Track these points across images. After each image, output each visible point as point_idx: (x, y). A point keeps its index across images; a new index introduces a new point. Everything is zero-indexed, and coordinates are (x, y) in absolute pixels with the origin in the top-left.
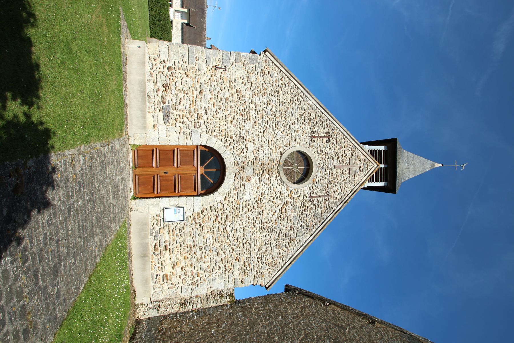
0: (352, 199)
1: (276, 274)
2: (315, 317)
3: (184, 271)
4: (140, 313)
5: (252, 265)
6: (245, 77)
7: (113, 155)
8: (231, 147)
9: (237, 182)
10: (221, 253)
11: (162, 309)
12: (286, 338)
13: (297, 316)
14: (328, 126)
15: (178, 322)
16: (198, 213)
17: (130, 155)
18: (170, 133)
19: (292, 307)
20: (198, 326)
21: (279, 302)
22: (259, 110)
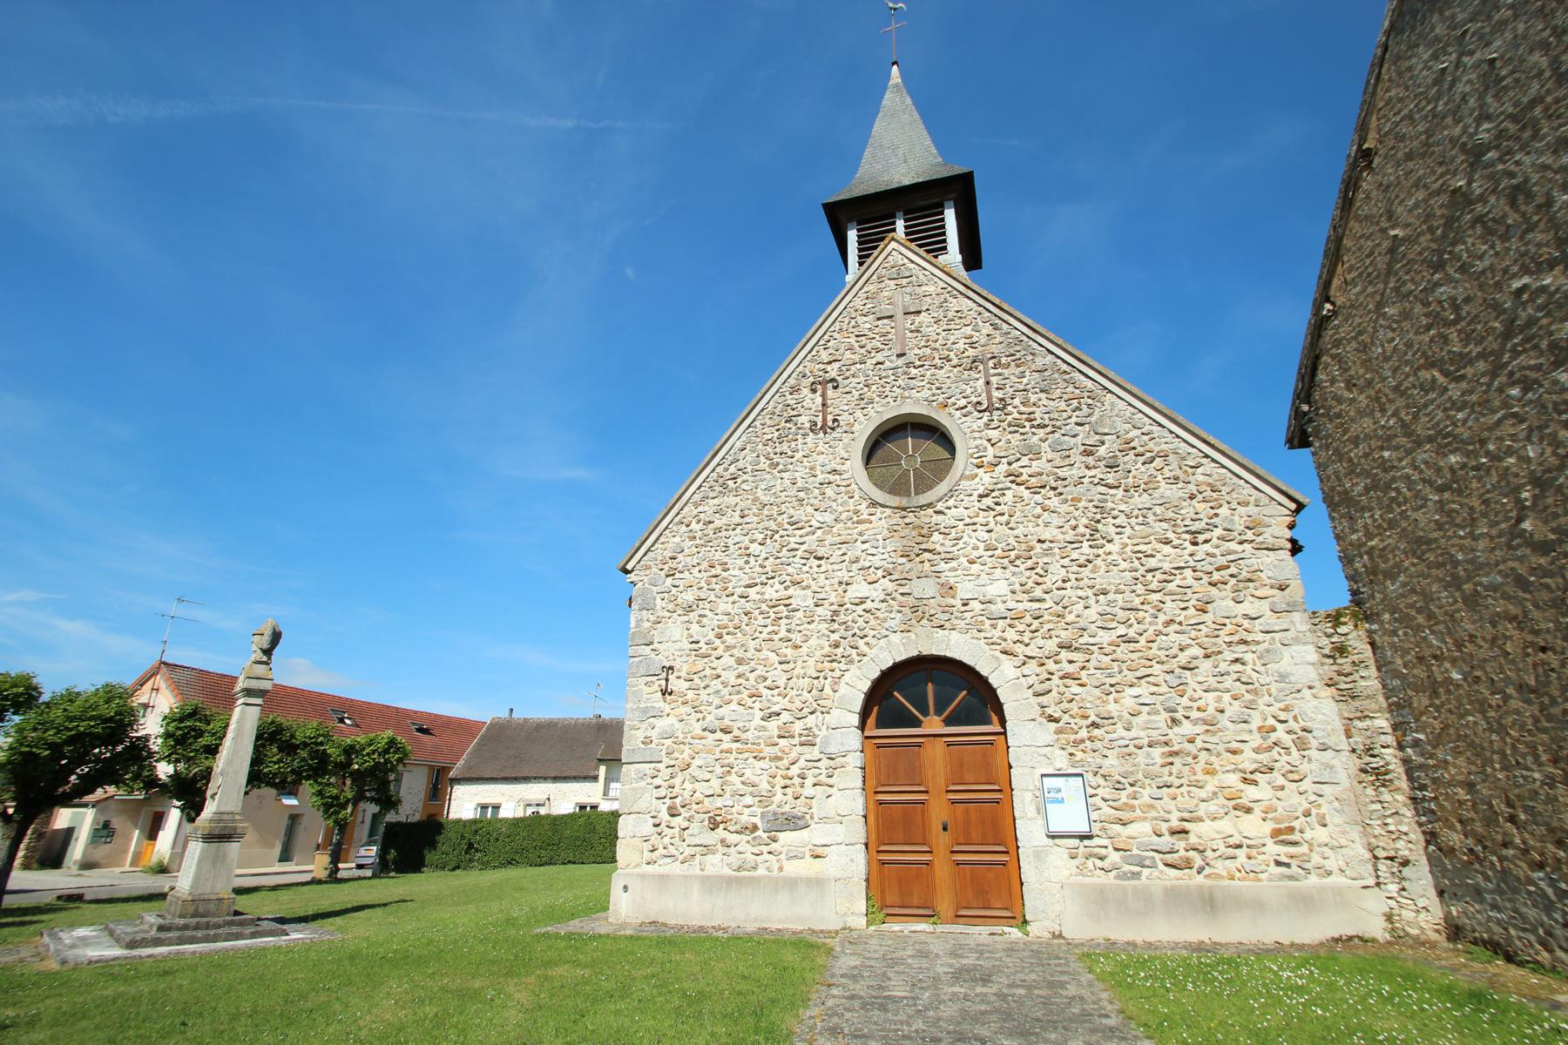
0: (990, 291)
1: (1247, 482)
2: (1373, 343)
3: (1258, 776)
4: (1422, 924)
5: (1223, 561)
6: (686, 618)
7: (866, 974)
8: (861, 643)
9: (959, 621)
10: (1183, 658)
11: (1402, 847)
12: (1447, 427)
13: (1377, 399)
14: (795, 390)
15: (1441, 794)
16: (1059, 732)
17: (896, 927)
18: (832, 814)
19: (1352, 420)
20: (1446, 727)
21: (1340, 461)
22: (764, 576)
